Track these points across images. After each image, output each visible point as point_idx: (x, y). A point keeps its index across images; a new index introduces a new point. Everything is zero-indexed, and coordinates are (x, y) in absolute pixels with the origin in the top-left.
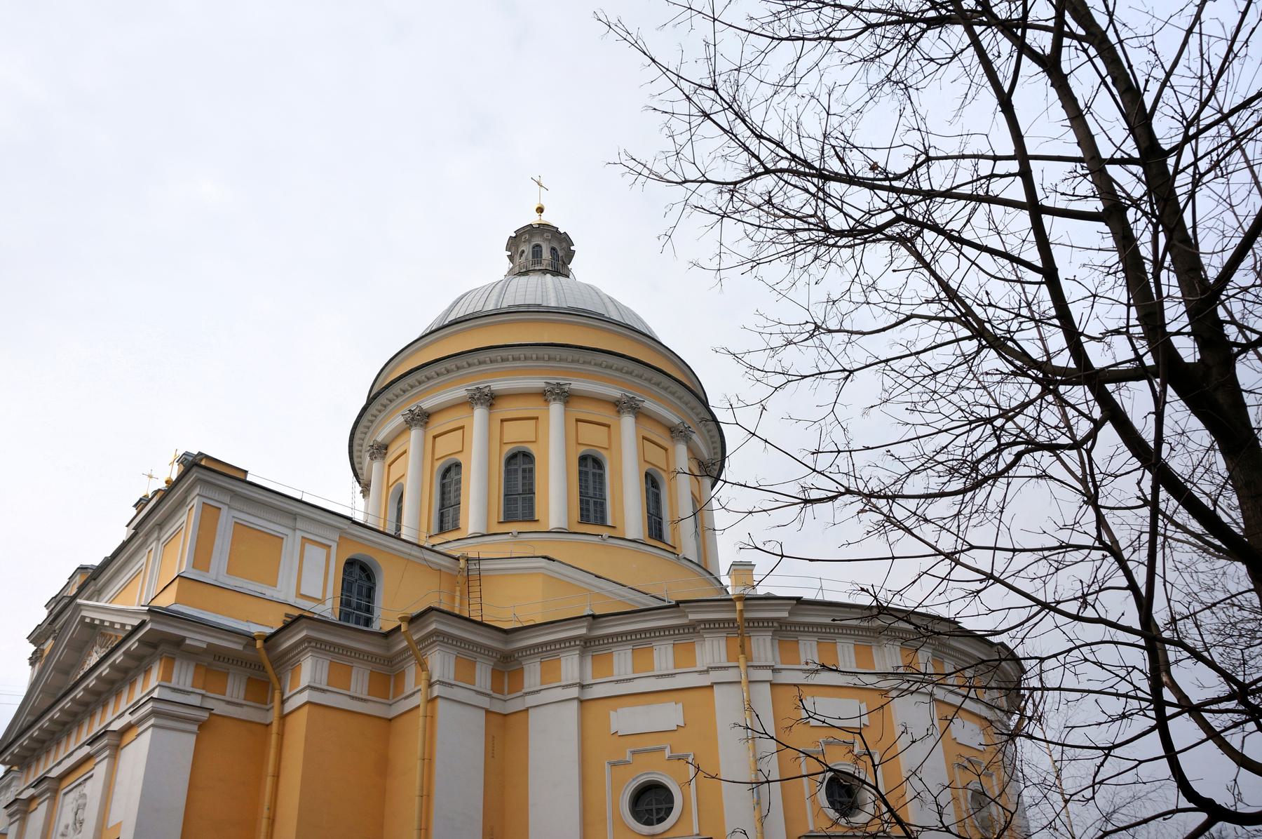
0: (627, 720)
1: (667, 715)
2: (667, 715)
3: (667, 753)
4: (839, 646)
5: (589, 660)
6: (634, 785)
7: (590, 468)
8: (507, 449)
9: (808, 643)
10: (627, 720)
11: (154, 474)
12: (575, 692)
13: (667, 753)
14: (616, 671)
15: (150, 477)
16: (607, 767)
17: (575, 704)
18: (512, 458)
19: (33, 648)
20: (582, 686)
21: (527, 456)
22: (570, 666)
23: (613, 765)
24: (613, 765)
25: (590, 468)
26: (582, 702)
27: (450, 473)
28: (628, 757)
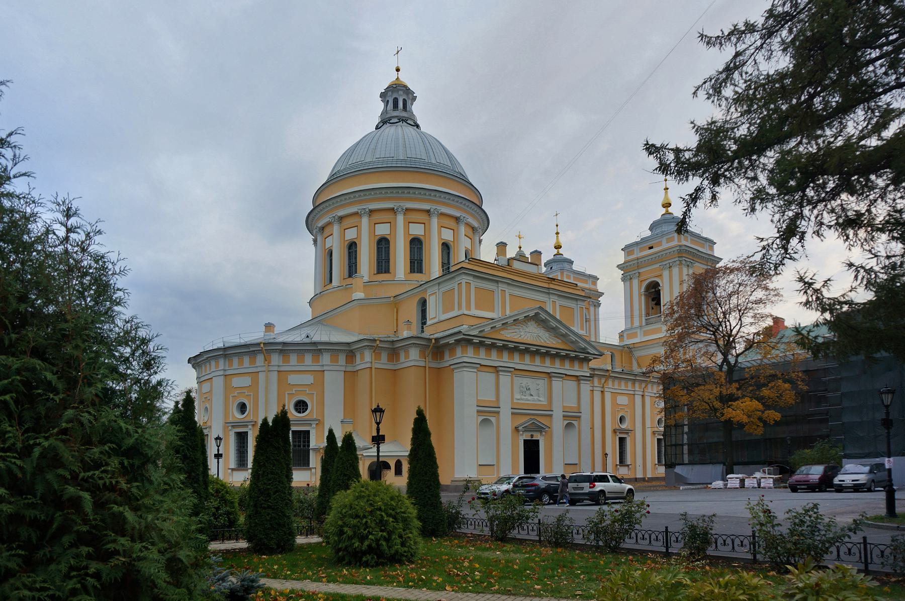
0: (293, 379)
1: (309, 379)
2: (309, 379)
7: (416, 244)
10: (293, 379)
22: (276, 359)
25: (416, 244)
27: (352, 247)
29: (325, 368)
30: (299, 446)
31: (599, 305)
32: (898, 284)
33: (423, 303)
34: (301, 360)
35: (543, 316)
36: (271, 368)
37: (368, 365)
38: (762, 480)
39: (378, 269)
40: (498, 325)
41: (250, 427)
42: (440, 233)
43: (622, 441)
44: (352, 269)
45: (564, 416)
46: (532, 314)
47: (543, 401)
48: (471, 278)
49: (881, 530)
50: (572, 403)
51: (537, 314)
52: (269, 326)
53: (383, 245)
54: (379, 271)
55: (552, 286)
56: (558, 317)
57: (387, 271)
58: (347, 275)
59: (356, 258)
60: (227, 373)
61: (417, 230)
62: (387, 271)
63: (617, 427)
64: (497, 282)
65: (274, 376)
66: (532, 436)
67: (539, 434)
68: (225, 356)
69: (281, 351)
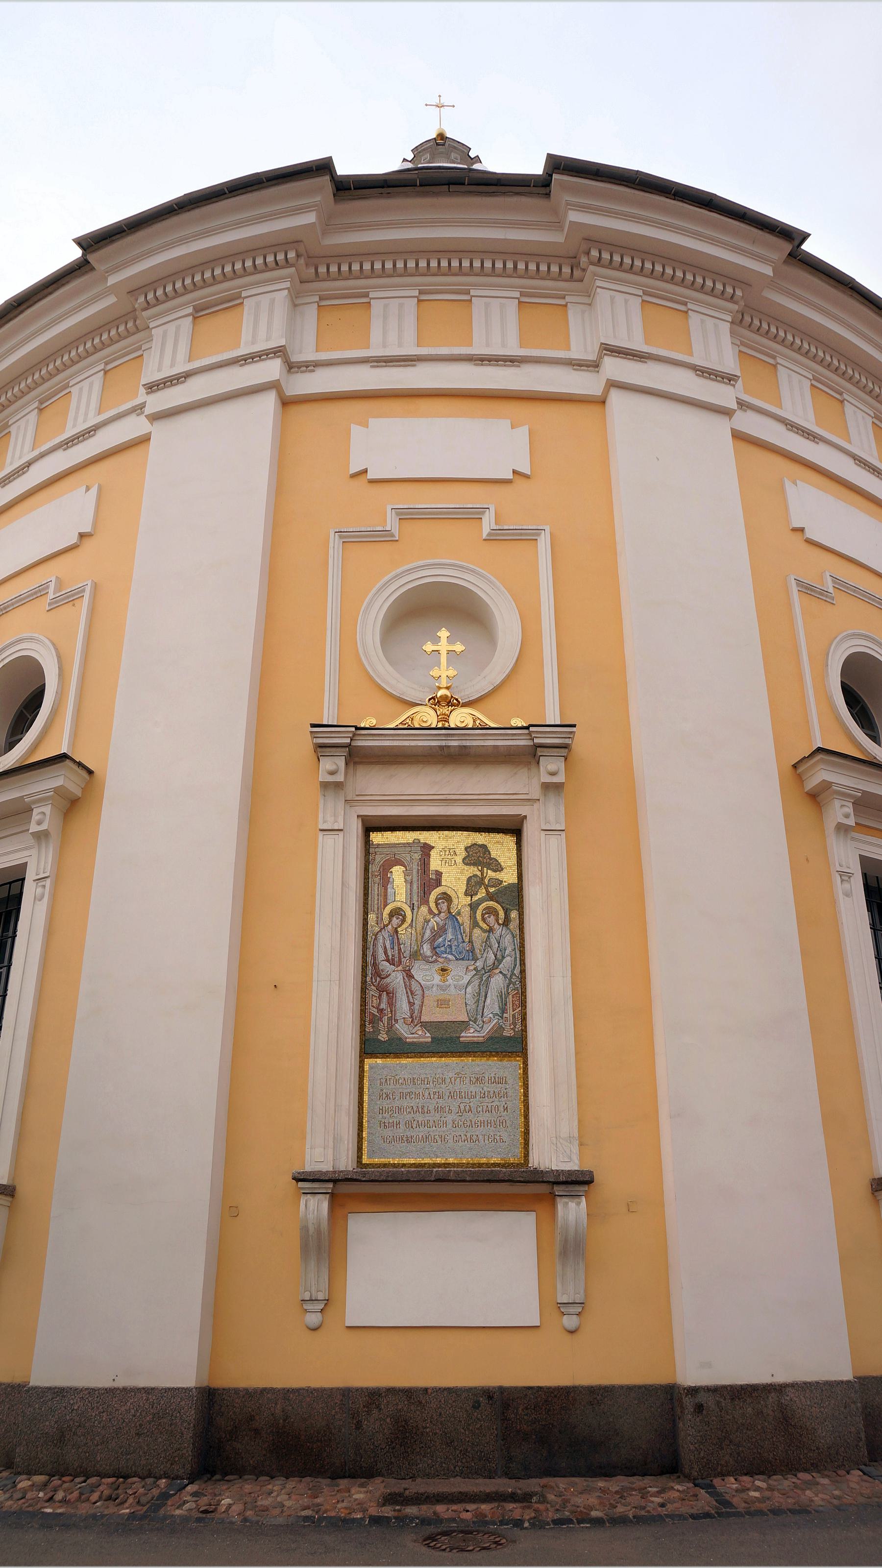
0: (391, 445)
2: (490, 446)
3: (488, 523)
4: (694, 320)
5: (311, 312)
6: (428, 576)
9: (495, 303)
11: (444, 101)
12: (272, 369)
13: (488, 523)
14: (376, 335)
15: (440, 106)
16: (335, 543)
17: (269, 402)
19: (76, 253)
20: (291, 367)
23: (349, 538)
24: (349, 538)
26: (286, 403)
28: (391, 523)
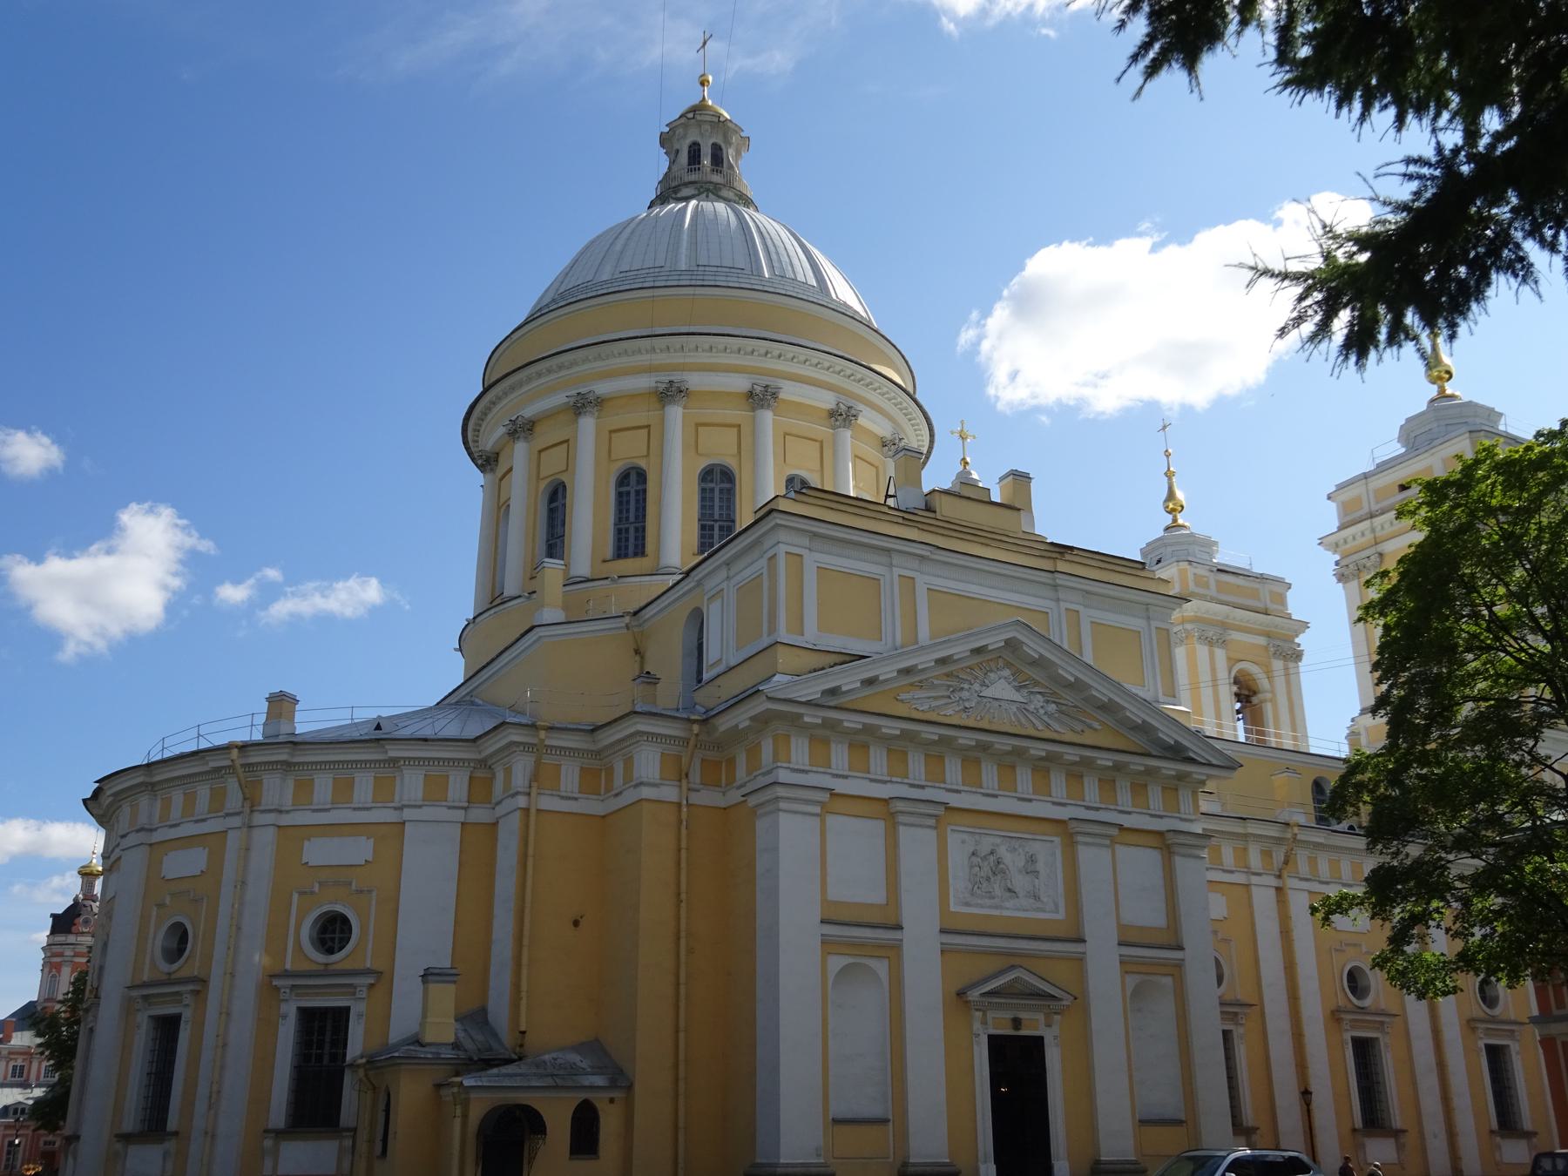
1: (358, 850)
6: (339, 908)
8: (703, 463)
18: (623, 479)
21: (642, 476)
23: (301, 893)
27: (557, 497)
29: (408, 814)
30: (320, 1058)
31: (1298, 656)
32: (1454, 72)
33: (697, 620)
34: (1043, 789)
35: (1033, 648)
36: (259, 819)
37: (522, 801)
38: (288, 802)
39: (619, 548)
40: (886, 671)
41: (188, 999)
42: (783, 455)
43: (1364, 1050)
44: (555, 543)
45: (826, 942)
46: (995, 641)
47: (1053, 912)
48: (806, 541)
49: (849, 1116)
50: (1148, 913)
51: (1011, 644)
52: (281, 704)
53: (632, 494)
54: (621, 552)
55: (1061, 566)
56: (1088, 658)
57: (640, 551)
58: (609, 550)
59: (563, 524)
60: (157, 837)
61: (720, 449)
62: (640, 551)
63: (1342, 1002)
64: (888, 551)
65: (265, 840)
66: (1017, 1023)
67: (1041, 1017)
68: (152, 788)
69: (288, 766)
